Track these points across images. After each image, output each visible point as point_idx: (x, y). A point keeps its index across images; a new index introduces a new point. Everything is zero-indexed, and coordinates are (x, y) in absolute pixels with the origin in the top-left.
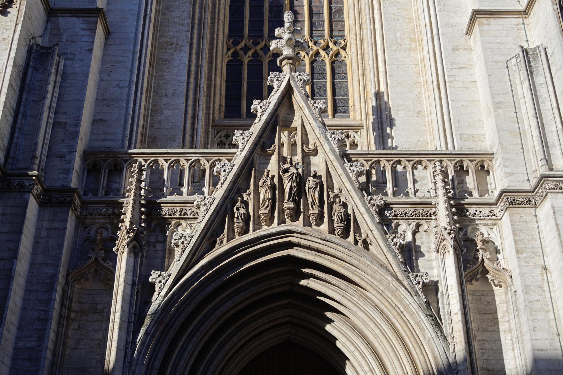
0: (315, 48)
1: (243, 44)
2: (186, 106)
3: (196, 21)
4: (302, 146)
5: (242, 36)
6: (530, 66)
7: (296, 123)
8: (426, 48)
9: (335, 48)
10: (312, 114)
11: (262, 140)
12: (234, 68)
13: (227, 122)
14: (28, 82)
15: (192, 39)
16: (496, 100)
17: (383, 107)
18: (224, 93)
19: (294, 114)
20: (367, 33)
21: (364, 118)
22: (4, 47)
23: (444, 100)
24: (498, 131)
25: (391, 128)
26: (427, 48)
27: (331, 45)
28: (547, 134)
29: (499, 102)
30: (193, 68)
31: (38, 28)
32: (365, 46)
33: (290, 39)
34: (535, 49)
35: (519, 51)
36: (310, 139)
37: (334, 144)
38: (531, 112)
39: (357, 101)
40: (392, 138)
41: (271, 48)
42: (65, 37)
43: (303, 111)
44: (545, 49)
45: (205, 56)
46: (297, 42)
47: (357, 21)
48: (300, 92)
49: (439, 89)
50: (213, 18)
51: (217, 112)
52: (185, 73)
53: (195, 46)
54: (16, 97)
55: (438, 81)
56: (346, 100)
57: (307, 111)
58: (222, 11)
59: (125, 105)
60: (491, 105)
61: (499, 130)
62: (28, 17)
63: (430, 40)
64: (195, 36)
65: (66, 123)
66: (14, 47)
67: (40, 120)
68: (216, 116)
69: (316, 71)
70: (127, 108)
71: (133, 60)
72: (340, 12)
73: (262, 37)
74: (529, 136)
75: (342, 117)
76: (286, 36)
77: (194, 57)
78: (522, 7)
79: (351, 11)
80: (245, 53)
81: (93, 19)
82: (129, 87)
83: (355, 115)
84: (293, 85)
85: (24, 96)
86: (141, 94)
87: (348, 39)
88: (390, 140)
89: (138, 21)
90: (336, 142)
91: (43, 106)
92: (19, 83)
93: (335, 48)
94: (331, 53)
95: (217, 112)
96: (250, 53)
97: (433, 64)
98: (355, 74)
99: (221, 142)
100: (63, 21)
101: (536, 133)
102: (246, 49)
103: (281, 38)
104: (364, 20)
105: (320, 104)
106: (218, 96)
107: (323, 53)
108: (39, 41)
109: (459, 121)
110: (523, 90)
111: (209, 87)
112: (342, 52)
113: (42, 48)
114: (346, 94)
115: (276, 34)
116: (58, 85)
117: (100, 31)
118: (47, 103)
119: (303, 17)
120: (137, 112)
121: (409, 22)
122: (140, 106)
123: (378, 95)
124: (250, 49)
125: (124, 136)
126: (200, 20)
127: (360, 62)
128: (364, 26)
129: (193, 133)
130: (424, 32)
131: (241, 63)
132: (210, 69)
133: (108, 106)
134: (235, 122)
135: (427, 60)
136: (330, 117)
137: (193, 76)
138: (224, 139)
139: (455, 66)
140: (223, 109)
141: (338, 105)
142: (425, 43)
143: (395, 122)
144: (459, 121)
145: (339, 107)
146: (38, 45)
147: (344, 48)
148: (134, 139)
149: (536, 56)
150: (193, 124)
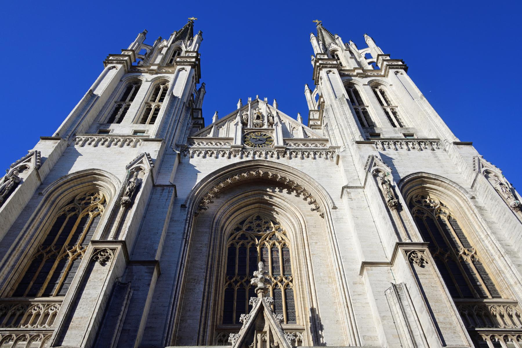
0: (275, 281)
1: (234, 279)
2: (201, 317)
3: (209, 267)
4: (270, 344)
5: (234, 274)
6: (399, 295)
7: (266, 329)
8: (338, 283)
9: (286, 281)
10: (275, 323)
11: (246, 340)
12: (229, 293)
13: (224, 327)
14: (110, 304)
15: (206, 276)
16: (383, 315)
17: (316, 317)
18: (223, 308)
19: (265, 323)
20: (304, 273)
21: (305, 324)
22: (100, 284)
23: (351, 314)
24: (386, 335)
25: (322, 331)
26: (338, 283)
27: (284, 279)
28: (415, 337)
29: (384, 316)
30: (206, 294)
31: (120, 273)
32: (304, 281)
33: (262, 278)
34: (400, 285)
35: (391, 285)
36: (274, 339)
37: (289, 342)
38: (403, 323)
39: (300, 313)
40: (323, 338)
41: (251, 283)
42: (135, 277)
43: (270, 321)
44: (405, 285)
45: (213, 286)
46: (266, 279)
47: (298, 266)
48: (268, 310)
49: (348, 307)
50: (218, 264)
51: (218, 320)
52: (202, 297)
53: (208, 281)
54: (102, 314)
55: (347, 302)
56: (294, 313)
57: (272, 321)
58: (223, 260)
59: (165, 317)
60: (379, 318)
61: (386, 333)
62: (116, 266)
63: (340, 278)
64: (208, 275)
65: (129, 330)
66: (106, 284)
67: (114, 328)
68: (218, 322)
69: (276, 295)
70: (167, 319)
71: (172, 290)
72: (288, 261)
73: (245, 274)
74: (404, 338)
75: (292, 323)
76: (260, 276)
77: (207, 287)
78: (389, 260)
79: (295, 261)
80: (236, 284)
81: (152, 266)
82: (169, 306)
83: (299, 322)
84: (264, 305)
85: (107, 313)
86: (176, 310)
87: (293, 276)
88: (321, 339)
89: (177, 267)
90: (290, 341)
91: (118, 319)
92: (105, 305)
93: (286, 281)
94: (284, 284)
95: (218, 320)
96: (238, 284)
97: (343, 292)
98: (298, 297)
99: (220, 339)
100: (136, 268)
101: (408, 336)
102: (236, 282)
103: (257, 277)
104: (302, 266)
105: (280, 317)
106: (219, 310)
107: (279, 284)
108: (120, 280)
109: (361, 328)
110: (396, 308)
111: (214, 305)
112: (290, 283)
113: (121, 284)
114: (294, 309)
115: (254, 275)
116: (127, 306)
117: (155, 273)
118: (120, 317)
119: (268, 263)
120: (172, 322)
121: (327, 267)
122: (174, 318)
123: (313, 310)
124: (238, 282)
125: (163, 337)
126: (211, 266)
127: (301, 290)
128: (302, 269)
129: (204, 334)
130: (336, 273)
131: (233, 290)
132: (216, 294)
133: (156, 318)
134: (229, 326)
135: (339, 290)
136: (285, 323)
137: (206, 298)
138: (222, 338)
139: (356, 294)
140: (222, 318)
141: (289, 315)
142: (337, 279)
143: (324, 327)
144: (361, 328)
145: (290, 317)
146: (119, 282)
147: (291, 281)
148: (169, 339)
149: (401, 289)
150: (204, 329)
